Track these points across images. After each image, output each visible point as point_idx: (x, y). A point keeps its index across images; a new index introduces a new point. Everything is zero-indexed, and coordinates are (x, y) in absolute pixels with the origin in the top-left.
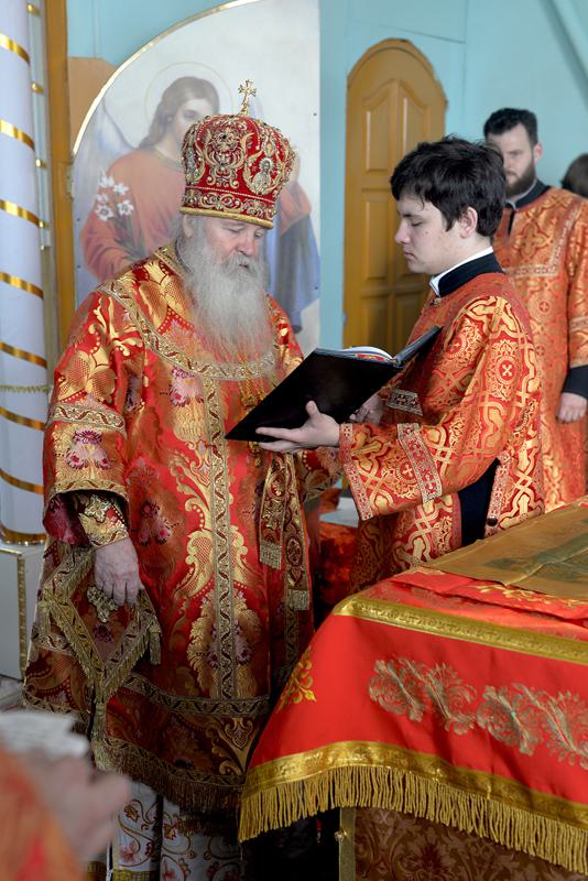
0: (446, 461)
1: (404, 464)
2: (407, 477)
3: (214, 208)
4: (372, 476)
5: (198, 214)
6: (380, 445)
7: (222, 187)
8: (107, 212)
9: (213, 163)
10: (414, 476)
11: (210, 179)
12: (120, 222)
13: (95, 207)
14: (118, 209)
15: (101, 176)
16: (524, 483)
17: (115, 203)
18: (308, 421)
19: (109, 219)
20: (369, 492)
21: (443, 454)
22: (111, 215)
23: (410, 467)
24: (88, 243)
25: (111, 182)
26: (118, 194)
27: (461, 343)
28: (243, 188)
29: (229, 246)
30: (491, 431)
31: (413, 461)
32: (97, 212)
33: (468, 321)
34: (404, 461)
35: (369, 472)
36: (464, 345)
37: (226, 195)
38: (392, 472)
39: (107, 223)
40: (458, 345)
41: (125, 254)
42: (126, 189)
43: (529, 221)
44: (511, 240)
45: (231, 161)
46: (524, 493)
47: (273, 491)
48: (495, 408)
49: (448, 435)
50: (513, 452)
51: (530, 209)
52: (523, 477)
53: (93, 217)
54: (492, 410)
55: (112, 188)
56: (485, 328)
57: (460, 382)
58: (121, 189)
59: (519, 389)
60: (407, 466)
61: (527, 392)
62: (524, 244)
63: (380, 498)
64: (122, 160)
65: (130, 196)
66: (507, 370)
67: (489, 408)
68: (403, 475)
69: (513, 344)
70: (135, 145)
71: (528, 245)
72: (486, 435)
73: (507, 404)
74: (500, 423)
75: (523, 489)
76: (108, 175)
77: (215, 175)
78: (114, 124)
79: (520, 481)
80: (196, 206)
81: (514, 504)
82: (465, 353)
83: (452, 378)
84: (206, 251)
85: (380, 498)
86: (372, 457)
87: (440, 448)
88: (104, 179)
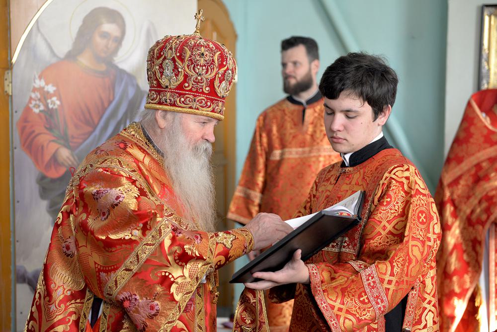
0: (392, 287)
1: (361, 293)
2: (363, 302)
3: (191, 108)
4: (337, 305)
5: (174, 111)
6: (346, 279)
7: (197, 92)
8: (39, 106)
9: (191, 73)
10: (369, 301)
11: (186, 85)
12: (49, 114)
13: (30, 102)
14: (48, 104)
15: (34, 79)
16: (429, 303)
17: (45, 99)
18: (292, 263)
19: (40, 111)
20: (338, 317)
21: (390, 282)
22: (42, 108)
23: (366, 294)
24: (23, 130)
25: (42, 83)
26: (48, 92)
27: (391, 198)
28: (213, 92)
29: (199, 135)
30: (414, 263)
31: (368, 290)
32: (31, 106)
33: (394, 182)
34: (362, 290)
35: (335, 301)
36: (393, 199)
37: (202, 98)
38: (352, 300)
39: (39, 115)
40: (389, 200)
41: (53, 139)
42: (55, 88)
43: (316, 115)
44: (305, 129)
45: (207, 72)
46: (430, 311)
47: (243, 320)
48: (416, 246)
49: (393, 267)
50: (421, 279)
51: (316, 106)
52: (429, 298)
53: (28, 110)
54: (414, 248)
55: (43, 88)
56: (406, 187)
57: (394, 227)
58: (51, 89)
59: (429, 232)
60: (363, 294)
61: (434, 233)
62: (315, 132)
63: (347, 321)
64: (51, 67)
65: (57, 94)
66: (423, 217)
67: (413, 246)
68: (360, 301)
69: (424, 198)
70: (62, 56)
71: (318, 132)
72: (411, 266)
73: (423, 243)
74: (419, 257)
75: (429, 307)
76: (40, 78)
77: (191, 82)
78: (46, 40)
79: (426, 301)
80: (174, 105)
81: (423, 318)
82: (394, 206)
83: (387, 225)
84: (182, 139)
85: (347, 321)
86: (338, 290)
87: (387, 278)
88: (37, 81)
